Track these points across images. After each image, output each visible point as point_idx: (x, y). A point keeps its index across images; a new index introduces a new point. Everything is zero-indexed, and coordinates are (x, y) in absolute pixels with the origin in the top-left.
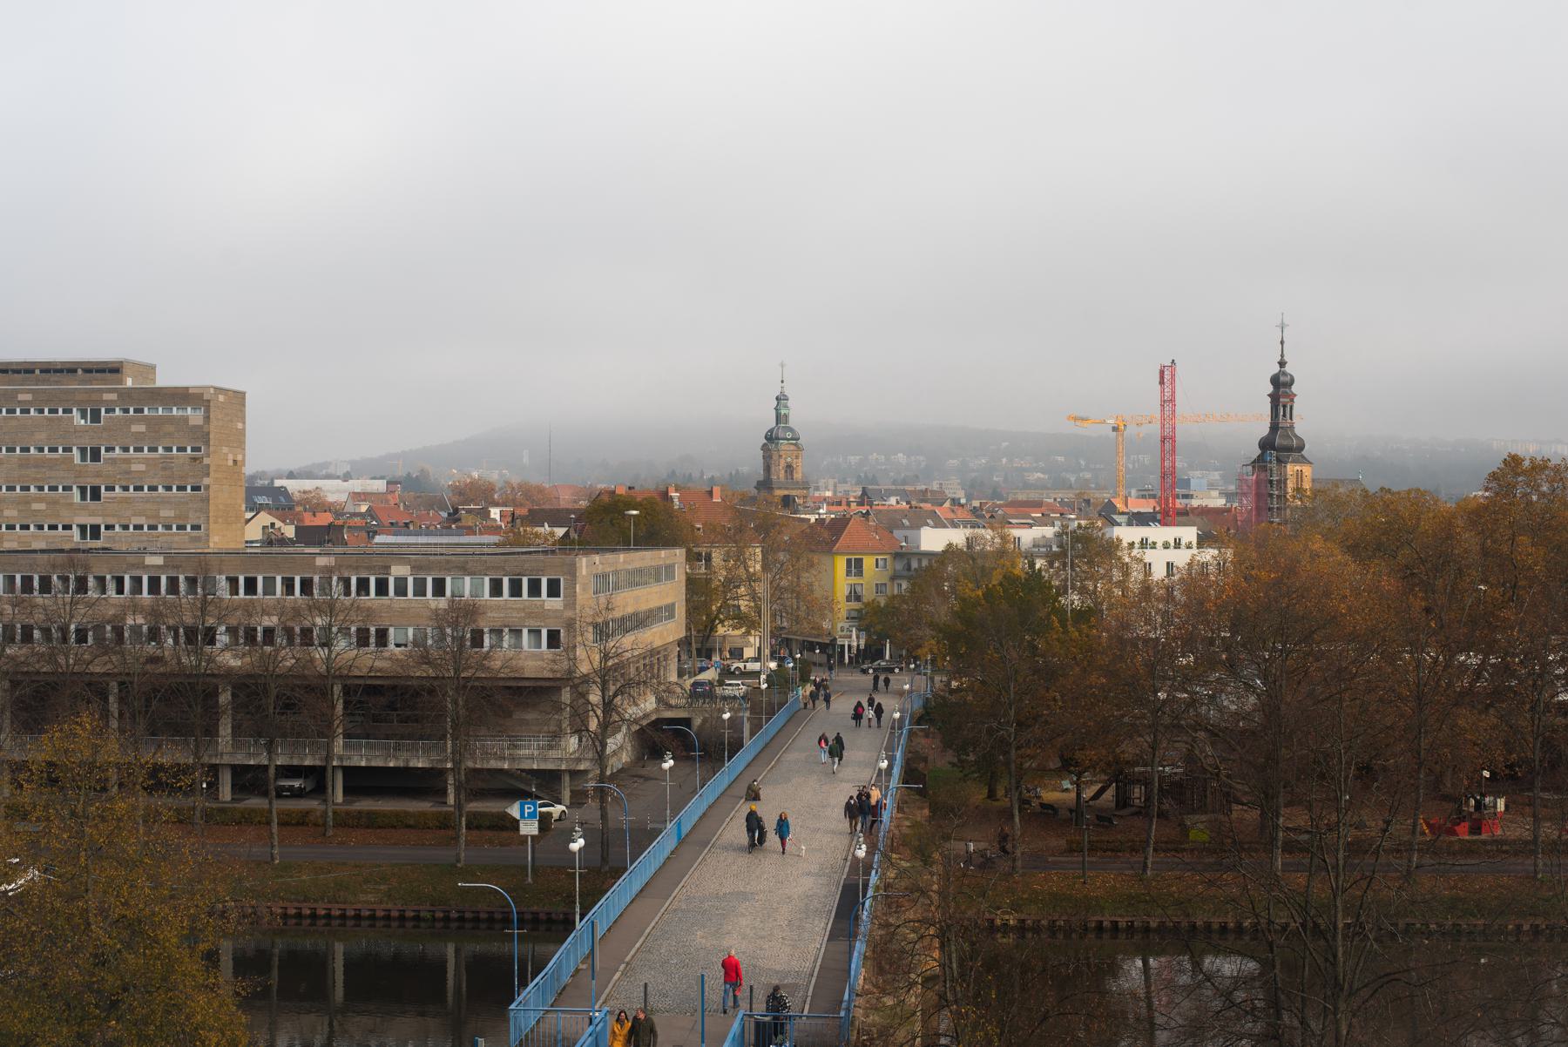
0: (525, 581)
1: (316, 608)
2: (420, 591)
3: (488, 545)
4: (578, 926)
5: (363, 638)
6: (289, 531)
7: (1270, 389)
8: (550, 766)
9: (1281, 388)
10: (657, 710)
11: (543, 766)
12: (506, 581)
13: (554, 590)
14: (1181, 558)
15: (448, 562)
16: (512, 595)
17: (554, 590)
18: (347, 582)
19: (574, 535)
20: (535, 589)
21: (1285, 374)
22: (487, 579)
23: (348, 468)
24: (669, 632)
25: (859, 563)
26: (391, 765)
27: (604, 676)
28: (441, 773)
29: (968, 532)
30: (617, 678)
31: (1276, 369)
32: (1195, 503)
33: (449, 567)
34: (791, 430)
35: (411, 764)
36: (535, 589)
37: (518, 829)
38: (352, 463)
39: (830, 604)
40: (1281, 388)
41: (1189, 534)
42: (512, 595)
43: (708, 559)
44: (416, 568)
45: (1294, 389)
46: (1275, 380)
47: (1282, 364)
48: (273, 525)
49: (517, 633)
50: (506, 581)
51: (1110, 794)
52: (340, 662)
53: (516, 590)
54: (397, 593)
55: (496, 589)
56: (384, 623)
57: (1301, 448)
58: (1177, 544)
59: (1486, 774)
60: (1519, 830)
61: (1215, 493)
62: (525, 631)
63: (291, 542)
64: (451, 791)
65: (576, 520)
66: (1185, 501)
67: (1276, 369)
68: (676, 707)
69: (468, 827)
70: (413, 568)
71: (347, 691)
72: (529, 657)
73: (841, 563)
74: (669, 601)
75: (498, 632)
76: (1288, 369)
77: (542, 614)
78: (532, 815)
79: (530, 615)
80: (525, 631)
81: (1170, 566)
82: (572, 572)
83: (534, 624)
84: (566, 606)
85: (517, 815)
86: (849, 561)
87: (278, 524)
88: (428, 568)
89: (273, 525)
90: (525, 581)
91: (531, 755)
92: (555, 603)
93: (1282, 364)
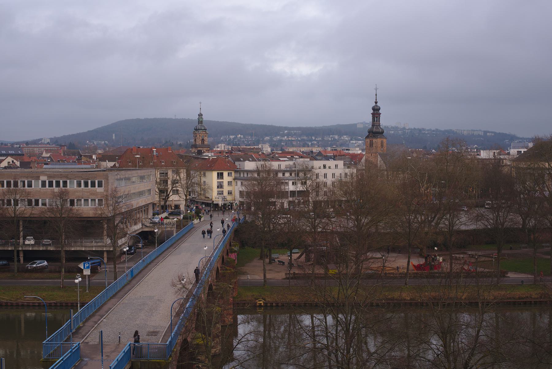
0: (89, 182)
2: (51, 184)
3: (50, 168)
4: (79, 311)
5: (30, 202)
7: (372, 111)
8: (99, 249)
9: (376, 112)
10: (142, 228)
12: (82, 182)
14: (338, 172)
15: (61, 175)
16: (64, 187)
17: (100, 185)
18: (24, 182)
19: (117, 165)
20: (93, 185)
21: (377, 106)
22: (75, 181)
23: (49, 141)
25: (222, 174)
26: (10, 249)
30: (130, 216)
31: (374, 104)
32: (351, 152)
33: (32, 178)
34: (204, 127)
36: (93, 185)
37: (83, 272)
38: (51, 139)
40: (376, 112)
41: (341, 163)
43: (167, 173)
44: (49, 177)
45: (380, 111)
46: (374, 109)
47: (376, 103)
49: (86, 200)
50: (82, 182)
51: (304, 256)
53: (86, 185)
54: (28, 186)
55: (79, 185)
56: (37, 198)
57: (382, 132)
58: (325, 167)
59: (436, 248)
60: (446, 267)
61: (358, 149)
62: (90, 200)
63: (17, 167)
65: (118, 159)
66: (347, 151)
67: (374, 104)
68: (149, 227)
69: (65, 272)
72: (87, 209)
73: (215, 174)
76: (378, 104)
77: (96, 194)
78: (88, 267)
79: (92, 194)
80: (90, 200)
81: (333, 175)
82: (107, 179)
83: (93, 197)
84: (104, 190)
85: (82, 268)
87: (15, 161)
88: (54, 177)
90: (89, 182)
92: (101, 190)
93: (376, 103)
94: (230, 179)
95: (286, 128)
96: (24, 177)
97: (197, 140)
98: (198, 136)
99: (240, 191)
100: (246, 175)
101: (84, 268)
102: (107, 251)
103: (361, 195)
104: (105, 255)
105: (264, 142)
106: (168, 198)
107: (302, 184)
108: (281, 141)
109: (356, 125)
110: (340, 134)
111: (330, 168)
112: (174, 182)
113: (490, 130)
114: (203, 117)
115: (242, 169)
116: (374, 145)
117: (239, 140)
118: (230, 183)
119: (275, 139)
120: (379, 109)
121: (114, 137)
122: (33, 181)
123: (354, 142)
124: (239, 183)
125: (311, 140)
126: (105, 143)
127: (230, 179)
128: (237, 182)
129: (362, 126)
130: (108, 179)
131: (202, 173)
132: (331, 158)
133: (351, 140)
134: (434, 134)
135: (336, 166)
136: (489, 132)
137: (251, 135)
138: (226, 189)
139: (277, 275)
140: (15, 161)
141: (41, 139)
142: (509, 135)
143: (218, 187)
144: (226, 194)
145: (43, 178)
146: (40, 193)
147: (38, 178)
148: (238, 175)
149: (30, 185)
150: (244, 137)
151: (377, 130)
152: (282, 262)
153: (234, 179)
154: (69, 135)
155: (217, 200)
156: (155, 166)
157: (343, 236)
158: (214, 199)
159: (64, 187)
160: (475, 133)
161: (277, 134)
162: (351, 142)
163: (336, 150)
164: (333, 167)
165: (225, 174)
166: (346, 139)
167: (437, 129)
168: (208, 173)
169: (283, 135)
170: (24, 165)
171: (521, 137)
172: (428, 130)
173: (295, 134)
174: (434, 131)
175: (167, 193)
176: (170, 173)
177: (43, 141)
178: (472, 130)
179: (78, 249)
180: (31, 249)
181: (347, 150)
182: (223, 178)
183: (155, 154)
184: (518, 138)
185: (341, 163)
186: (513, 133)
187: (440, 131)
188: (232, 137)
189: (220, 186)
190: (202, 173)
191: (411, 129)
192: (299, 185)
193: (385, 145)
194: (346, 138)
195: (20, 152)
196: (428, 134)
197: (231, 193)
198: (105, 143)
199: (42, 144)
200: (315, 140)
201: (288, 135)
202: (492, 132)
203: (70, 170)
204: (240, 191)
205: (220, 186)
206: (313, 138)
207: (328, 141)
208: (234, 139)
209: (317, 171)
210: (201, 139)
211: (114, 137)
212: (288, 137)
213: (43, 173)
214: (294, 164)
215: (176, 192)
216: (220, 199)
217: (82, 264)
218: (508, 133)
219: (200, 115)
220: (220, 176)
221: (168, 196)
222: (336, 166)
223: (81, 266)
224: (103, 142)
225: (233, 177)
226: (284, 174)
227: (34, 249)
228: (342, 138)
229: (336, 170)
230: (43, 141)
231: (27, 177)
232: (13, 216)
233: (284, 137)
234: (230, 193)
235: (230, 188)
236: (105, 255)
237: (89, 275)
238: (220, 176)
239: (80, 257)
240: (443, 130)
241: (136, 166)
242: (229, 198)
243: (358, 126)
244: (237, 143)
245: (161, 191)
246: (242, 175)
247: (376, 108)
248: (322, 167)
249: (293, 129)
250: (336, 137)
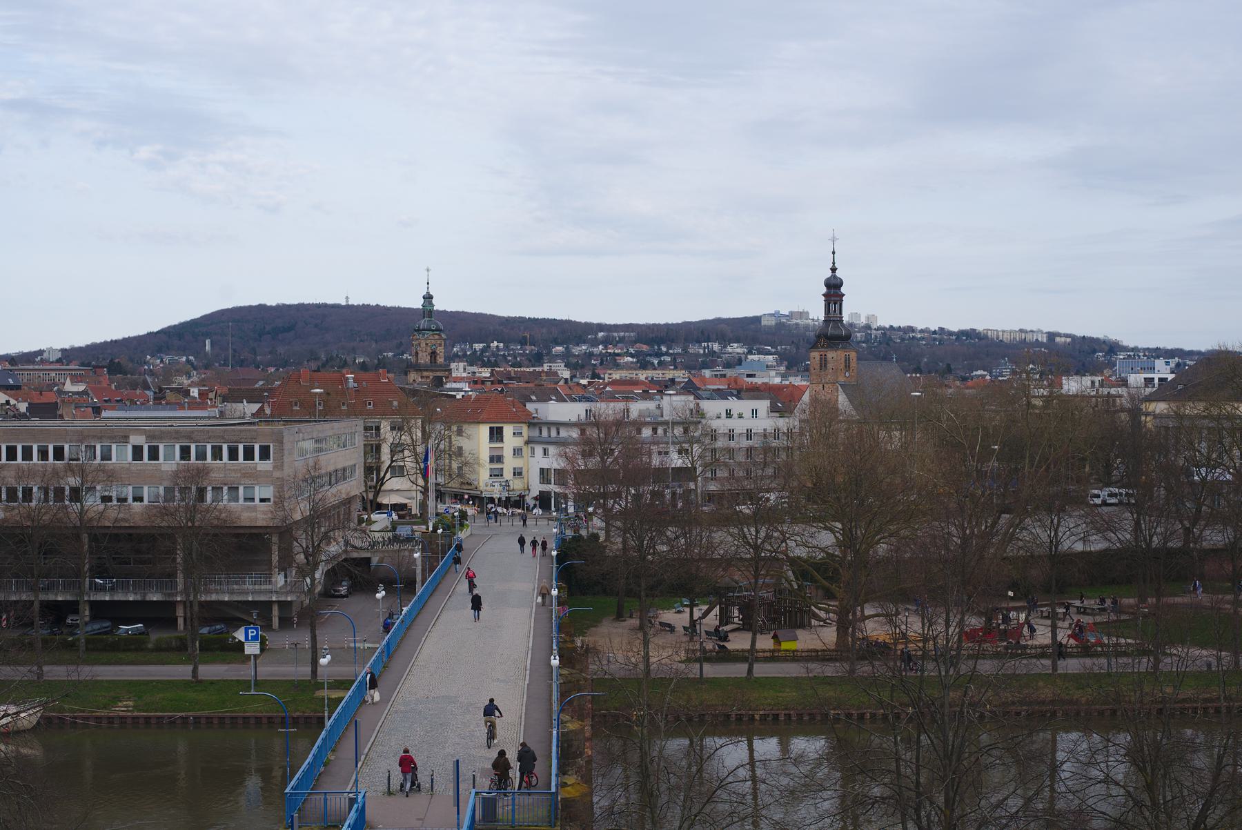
1: (70, 469)
6: (23, 407)
7: (824, 290)
8: (263, 598)
9: (834, 290)
10: (345, 551)
11: (257, 598)
12: (225, 447)
13: (265, 453)
15: (177, 432)
16: (230, 459)
20: (249, 454)
21: (834, 277)
24: (354, 486)
25: (500, 430)
26: (60, 599)
27: (311, 521)
28: (174, 604)
29: (587, 405)
31: (829, 274)
32: (758, 381)
33: (113, 439)
35: (148, 599)
36: (249, 454)
39: (477, 461)
40: (834, 290)
41: (763, 405)
42: (230, 459)
43: (378, 428)
44: (150, 436)
45: (843, 290)
47: (834, 270)
48: (8, 403)
50: (225, 447)
51: (716, 610)
52: (91, 514)
53: (233, 455)
58: (729, 414)
59: (1010, 594)
61: (773, 373)
62: (225, 488)
64: (181, 621)
66: (749, 380)
70: (147, 437)
71: (94, 538)
73: (484, 430)
74: (351, 463)
75: (217, 489)
76: (838, 274)
78: (255, 638)
80: (225, 488)
82: (280, 442)
84: (274, 467)
85: (243, 639)
86: (492, 429)
87: (13, 402)
89: (8, 403)
91: (249, 590)
92: (266, 465)
93: (834, 270)
94: (519, 442)
95: (601, 327)
96: (94, 437)
97: (420, 355)
98: (423, 345)
99: (542, 470)
100: (554, 433)
101: (247, 638)
102: (279, 602)
103: (833, 478)
104: (276, 611)
105: (553, 358)
106: (382, 484)
107: (680, 452)
108: (591, 355)
109: (757, 319)
110: (725, 340)
111: (740, 416)
112: (396, 449)
113: (1062, 331)
114: (434, 301)
115: (544, 420)
116: (830, 366)
117: (493, 354)
118: (517, 452)
119: (576, 350)
120: (841, 284)
121: (208, 348)
122: (114, 447)
123: (756, 357)
124: (539, 450)
125: (659, 354)
126: (188, 361)
127: (519, 442)
128: (533, 449)
129: (772, 322)
130: (282, 443)
131: (454, 428)
132: (732, 395)
133: (750, 352)
134: (935, 339)
135: (754, 413)
136: (1059, 335)
137: (523, 342)
138: (510, 463)
139: (665, 655)
140: (13, 402)
141: (41, 352)
142: (780, 326)
143: (492, 460)
144: (508, 474)
145: (137, 439)
146: (133, 470)
147: (125, 439)
148: (536, 433)
149: (106, 456)
150: (506, 348)
151: (837, 332)
152: (669, 625)
153: (527, 443)
154: (106, 343)
155: (489, 488)
156: (353, 412)
157: (804, 569)
158: (482, 487)
159: (182, 458)
160: (1030, 337)
161: (580, 341)
162: (750, 357)
163: (724, 376)
164: (747, 414)
165: (508, 430)
166: (739, 350)
167: (942, 329)
168: (468, 429)
169: (595, 343)
170: (38, 410)
171: (1132, 345)
172: (922, 331)
173: (622, 340)
174: (935, 332)
175: (378, 474)
176: (385, 426)
177: (45, 355)
178: (1021, 331)
179: (214, 597)
180: (107, 598)
181: (749, 376)
182: (502, 441)
183: (351, 384)
184: (1125, 349)
185: (763, 405)
186: (1113, 337)
187: (950, 333)
188: (478, 346)
189: (496, 459)
190: (454, 428)
191: (884, 329)
192: (675, 455)
193: (853, 364)
194: (736, 349)
195: (11, 381)
196: (923, 338)
197: (520, 474)
198: (188, 361)
199: (42, 361)
200: (667, 354)
201: (606, 342)
202: (1067, 336)
203: (194, 422)
204: (542, 470)
205: (496, 459)
206: (664, 349)
207: (698, 355)
208: (483, 351)
209: (715, 424)
210: (429, 350)
211: (208, 348)
212: (606, 348)
213: (137, 430)
214: (659, 407)
215: (398, 471)
216: (497, 488)
217: (242, 630)
218: (1101, 336)
219: (428, 298)
220: (497, 435)
221: (381, 481)
222: (754, 413)
223: (240, 635)
224: (184, 359)
225: (526, 437)
226: (655, 430)
227: (116, 598)
228: (729, 349)
229: (755, 420)
230: (45, 355)
231: (100, 439)
232: (78, 524)
233: (597, 346)
234: (518, 473)
235: (518, 463)
236: (276, 611)
237: (255, 656)
238: (497, 435)
239: (233, 615)
240: (955, 329)
241: (313, 414)
242: (517, 485)
243: (764, 322)
244: (493, 359)
245: (369, 470)
246: (545, 433)
247: (833, 282)
248: (724, 415)
249: (616, 328)
250: (716, 347)
